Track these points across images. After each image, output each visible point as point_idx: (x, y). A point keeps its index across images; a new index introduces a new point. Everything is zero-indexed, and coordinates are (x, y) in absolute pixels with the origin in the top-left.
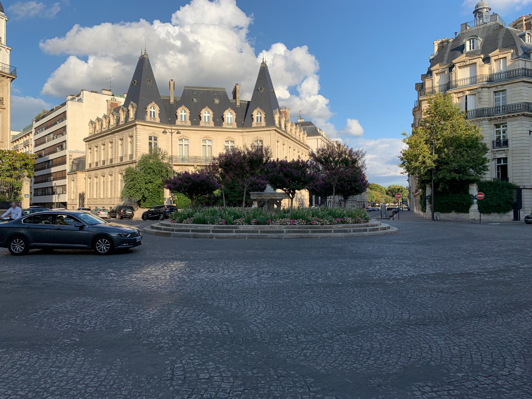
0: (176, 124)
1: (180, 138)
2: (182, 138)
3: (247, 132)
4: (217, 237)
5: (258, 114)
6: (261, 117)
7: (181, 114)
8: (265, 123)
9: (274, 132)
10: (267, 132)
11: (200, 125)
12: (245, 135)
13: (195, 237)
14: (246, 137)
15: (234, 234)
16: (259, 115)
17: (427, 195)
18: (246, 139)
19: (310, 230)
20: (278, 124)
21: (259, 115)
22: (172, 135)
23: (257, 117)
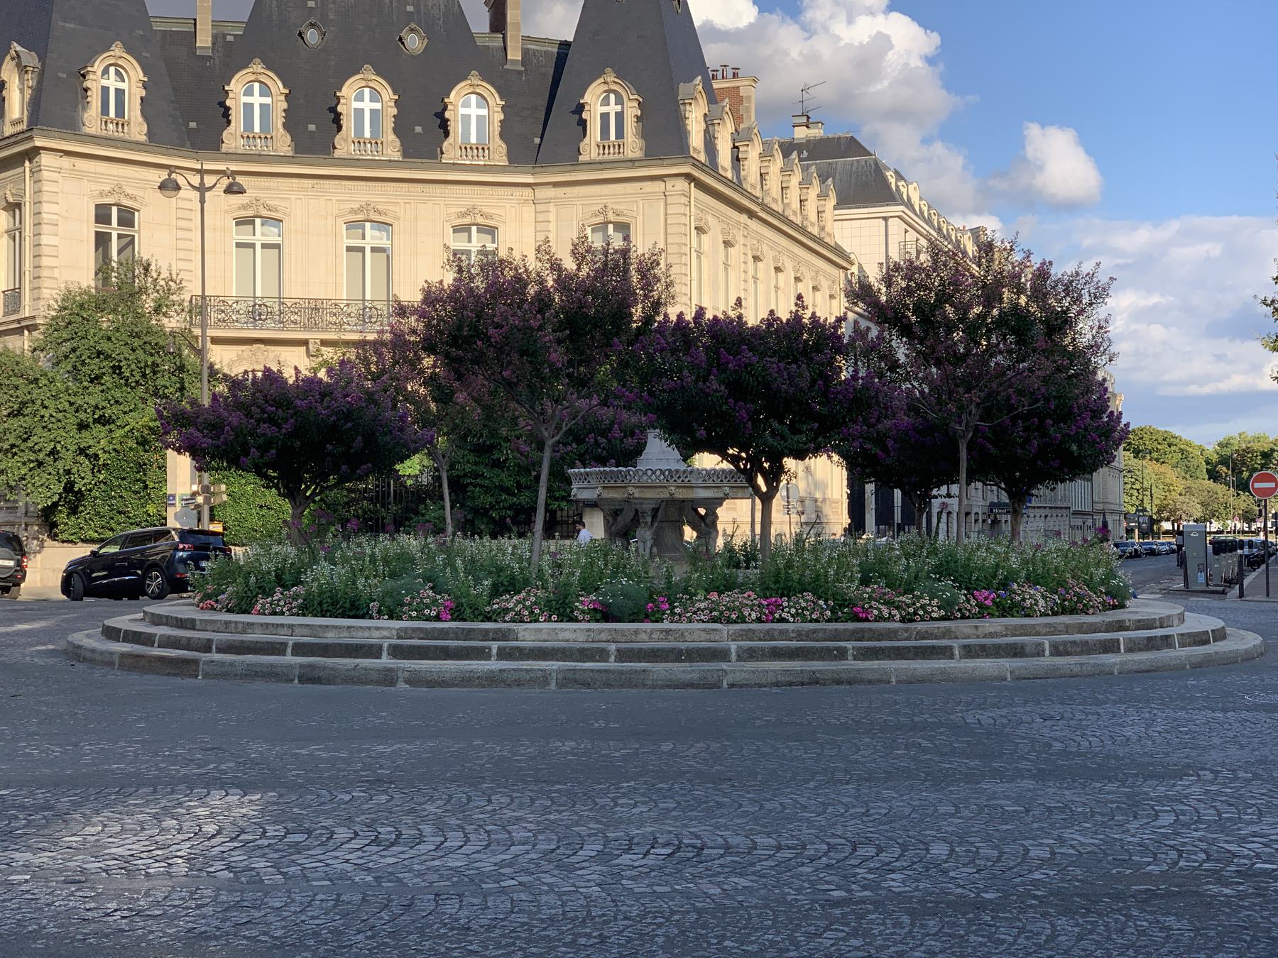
0: (224, 148)
2: (251, 212)
3: (556, 185)
4: (416, 680)
5: (606, 102)
7: (248, 99)
8: (640, 143)
9: (681, 184)
10: (649, 186)
11: (337, 153)
12: (548, 201)
13: (310, 677)
14: (552, 207)
15: (494, 665)
16: (613, 108)
19: (849, 645)
21: (613, 108)
22: (202, 201)
23: (605, 117)
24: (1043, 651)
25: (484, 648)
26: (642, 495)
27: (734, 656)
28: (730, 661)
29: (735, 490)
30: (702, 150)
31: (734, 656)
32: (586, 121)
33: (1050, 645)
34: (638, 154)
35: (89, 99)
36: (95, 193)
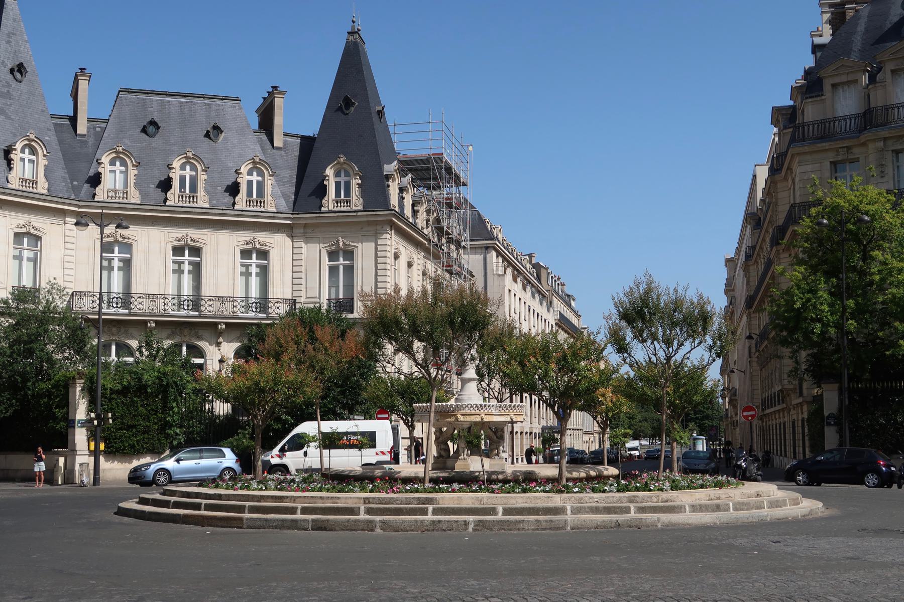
1: (177, 243)
4: (385, 525)
6: (261, 185)
7: (250, 178)
8: (137, 193)
13: (319, 526)
15: (430, 517)
16: (188, 172)
17: (826, 413)
18: (303, 251)
20: (397, 205)
21: (188, 172)
23: (250, 183)
24: (729, 508)
25: (425, 508)
26: (466, 420)
27: (569, 512)
28: (567, 515)
29: (517, 416)
30: (397, 205)
31: (569, 512)
32: (326, 185)
33: (733, 505)
34: (360, 208)
35: (12, 166)
36: (14, 226)
